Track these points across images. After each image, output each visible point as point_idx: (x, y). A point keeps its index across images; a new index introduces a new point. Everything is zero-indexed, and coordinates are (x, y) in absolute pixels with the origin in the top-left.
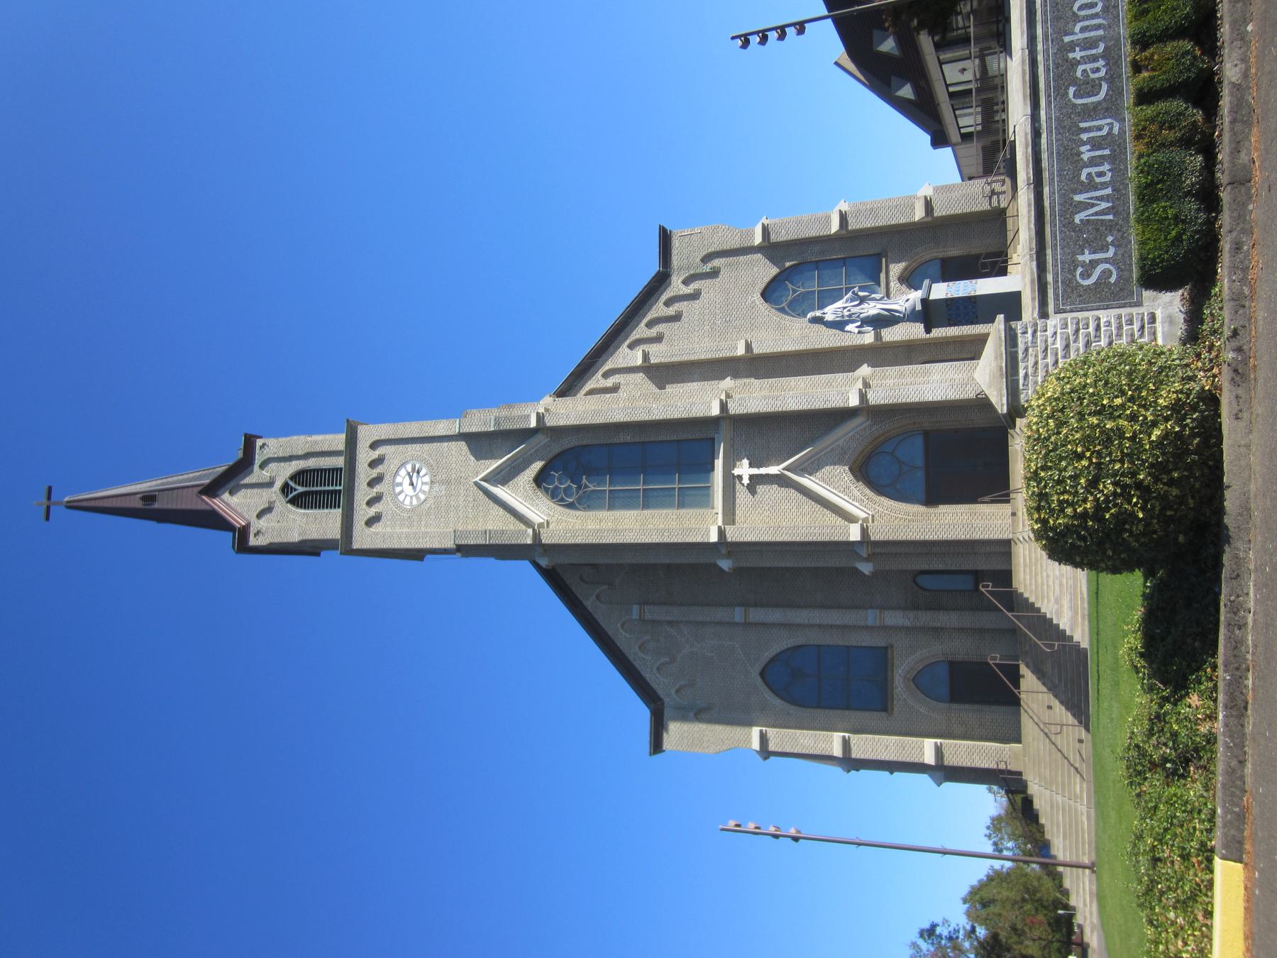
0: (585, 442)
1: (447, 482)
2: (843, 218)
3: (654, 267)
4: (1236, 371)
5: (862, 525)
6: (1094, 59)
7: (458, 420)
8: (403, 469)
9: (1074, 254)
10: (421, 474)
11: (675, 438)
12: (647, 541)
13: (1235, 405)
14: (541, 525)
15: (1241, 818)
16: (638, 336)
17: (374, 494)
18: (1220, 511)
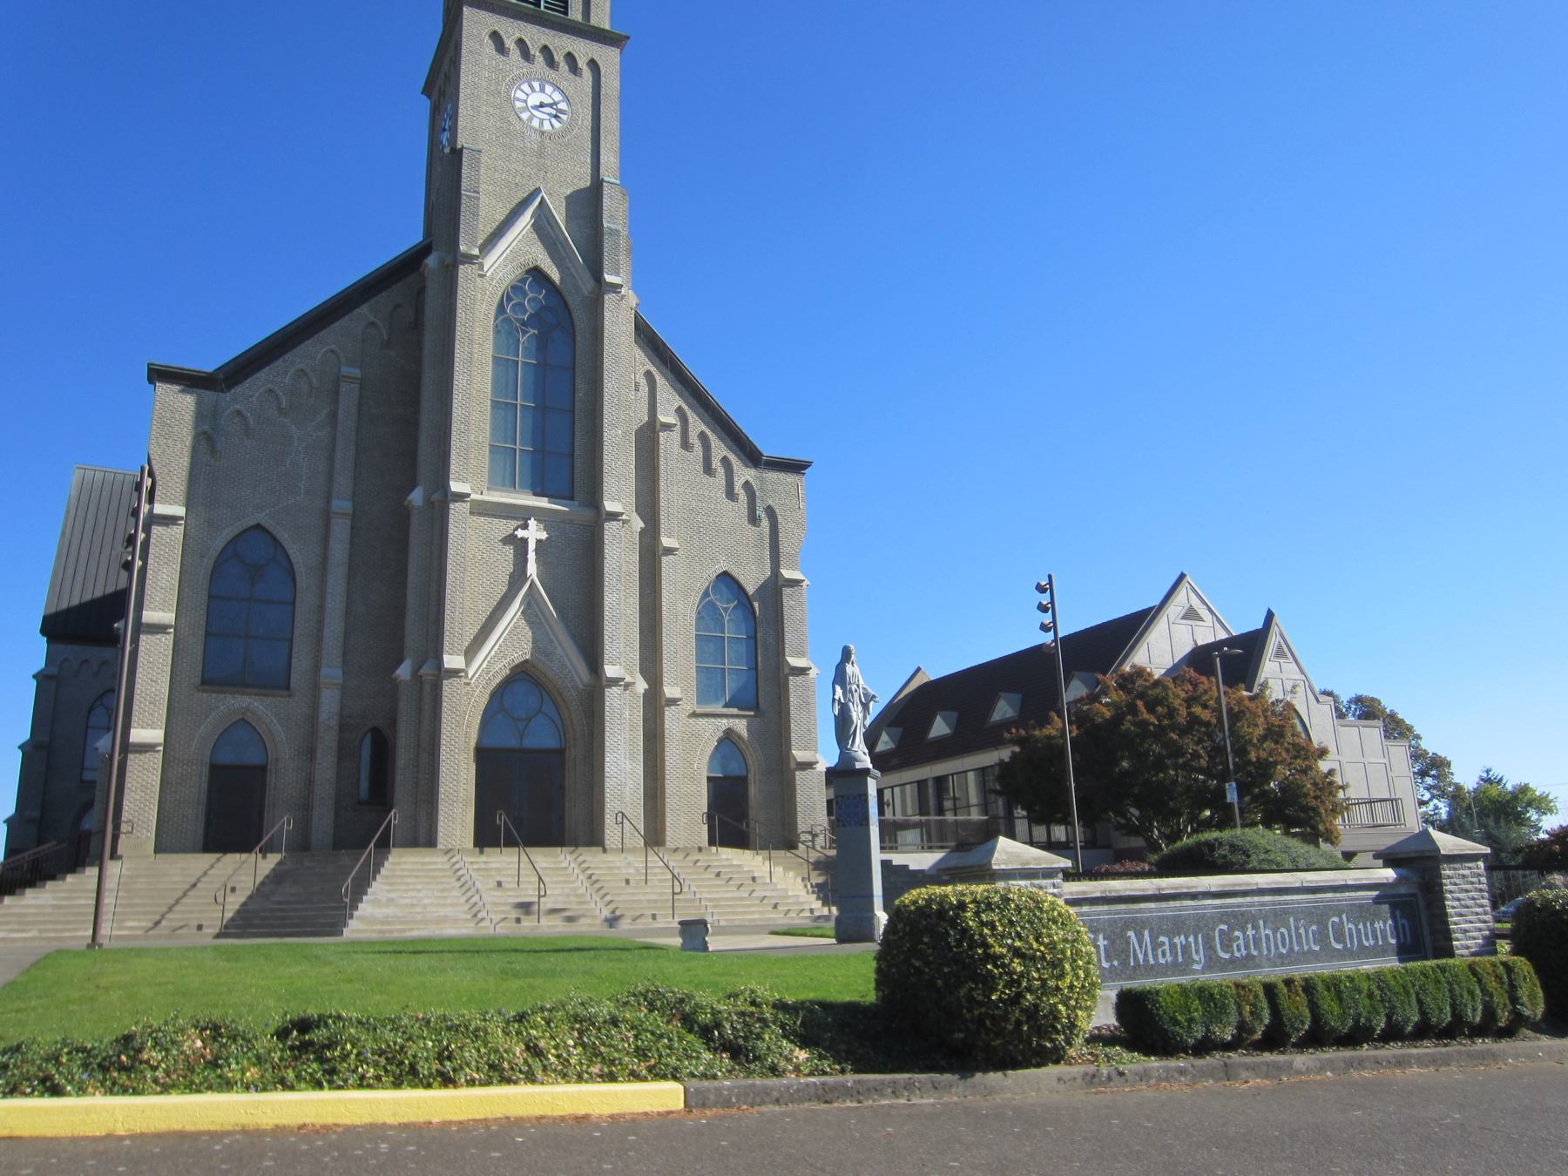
0: (578, 338)
1: (541, 154)
2: (802, 671)
3: (768, 450)
4: (1094, 1076)
5: (462, 671)
6: (1247, 947)
7: (618, 182)
8: (561, 98)
9: (1104, 931)
10: (553, 120)
11: (577, 452)
12: (455, 401)
13: (1069, 1077)
14: (481, 266)
15: (727, 1104)
16: (691, 420)
17: (532, 52)
18: (985, 1070)
